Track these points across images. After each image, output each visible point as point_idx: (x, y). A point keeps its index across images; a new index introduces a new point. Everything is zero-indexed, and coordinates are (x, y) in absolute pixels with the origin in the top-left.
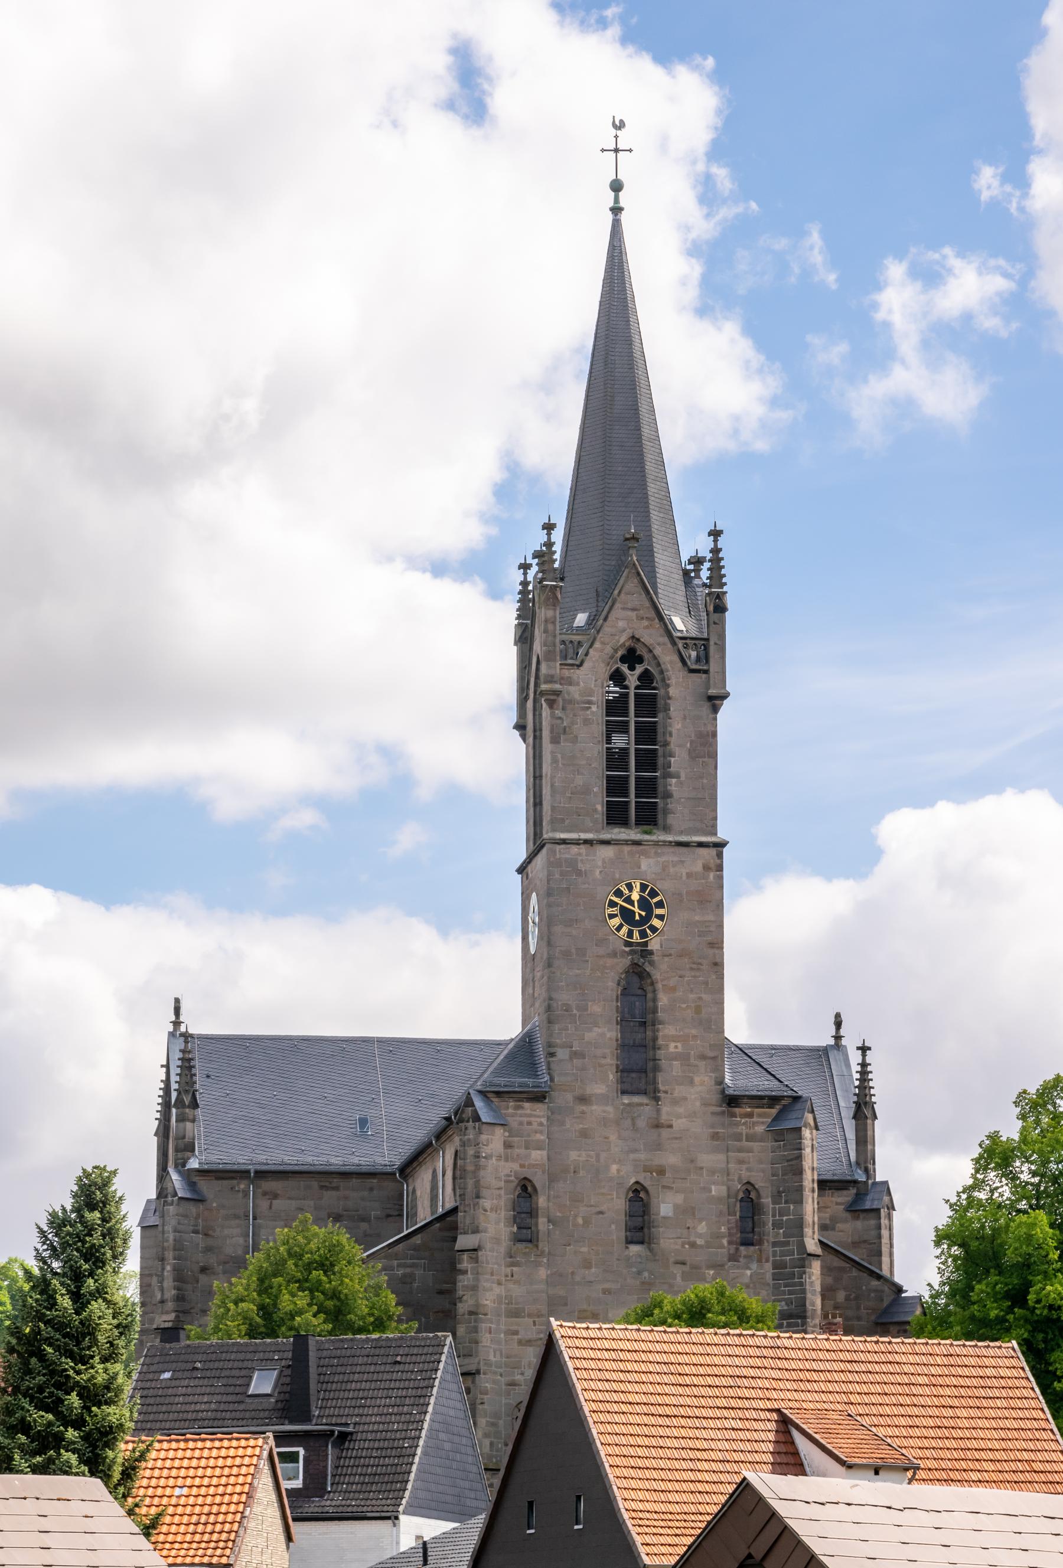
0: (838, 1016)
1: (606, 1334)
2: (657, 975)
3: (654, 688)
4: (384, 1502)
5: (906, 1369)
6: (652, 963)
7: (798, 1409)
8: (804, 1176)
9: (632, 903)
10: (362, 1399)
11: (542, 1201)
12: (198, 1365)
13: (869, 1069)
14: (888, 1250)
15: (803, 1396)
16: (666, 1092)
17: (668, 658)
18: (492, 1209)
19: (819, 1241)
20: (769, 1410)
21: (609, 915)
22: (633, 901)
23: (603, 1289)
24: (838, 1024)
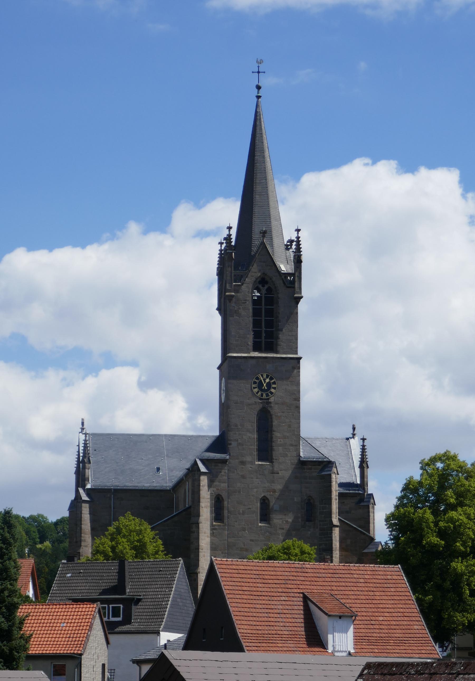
0: (353, 426)
1: (234, 563)
2: (272, 412)
3: (273, 294)
4: (154, 626)
5: (355, 576)
6: (271, 407)
7: (310, 592)
8: (332, 494)
9: (265, 382)
10: (146, 585)
11: (226, 503)
12: (82, 571)
13: (366, 447)
14: (373, 521)
15: (313, 587)
16: (276, 459)
17: (278, 282)
18: (205, 507)
19: (339, 519)
20: (299, 593)
21: (253, 387)
22: (266, 382)
23: (250, 539)
24: (354, 429)
